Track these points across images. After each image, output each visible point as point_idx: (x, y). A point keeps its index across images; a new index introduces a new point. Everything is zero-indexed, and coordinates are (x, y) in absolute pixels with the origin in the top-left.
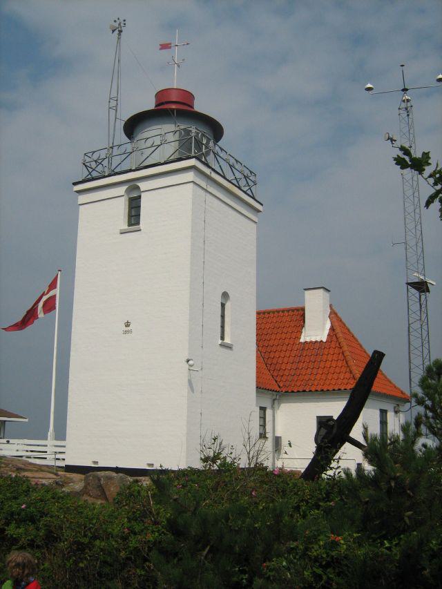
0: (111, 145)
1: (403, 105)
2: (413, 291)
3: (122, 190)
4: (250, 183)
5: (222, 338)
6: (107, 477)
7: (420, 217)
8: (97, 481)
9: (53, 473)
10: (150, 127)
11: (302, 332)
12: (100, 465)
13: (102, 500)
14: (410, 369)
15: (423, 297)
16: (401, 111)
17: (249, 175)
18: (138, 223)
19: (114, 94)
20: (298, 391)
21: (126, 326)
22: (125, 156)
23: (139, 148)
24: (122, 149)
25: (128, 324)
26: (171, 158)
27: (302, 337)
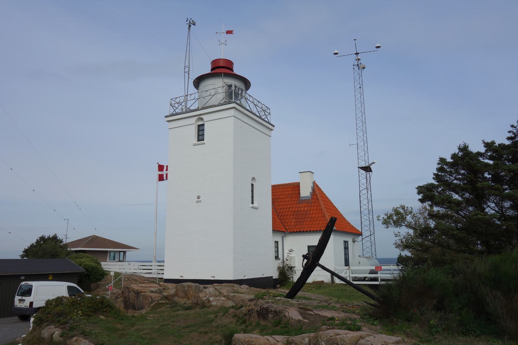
0: (186, 94)
1: (356, 63)
2: (363, 172)
4: (267, 114)
5: (252, 203)
6: (188, 286)
7: (362, 81)
12: (184, 278)
14: (360, 201)
15: (368, 175)
17: (266, 109)
18: (203, 140)
19: (187, 64)
20: (297, 232)
21: (198, 198)
22: (194, 101)
23: (219, 93)
24: (193, 97)
25: (199, 197)
26: (222, 102)
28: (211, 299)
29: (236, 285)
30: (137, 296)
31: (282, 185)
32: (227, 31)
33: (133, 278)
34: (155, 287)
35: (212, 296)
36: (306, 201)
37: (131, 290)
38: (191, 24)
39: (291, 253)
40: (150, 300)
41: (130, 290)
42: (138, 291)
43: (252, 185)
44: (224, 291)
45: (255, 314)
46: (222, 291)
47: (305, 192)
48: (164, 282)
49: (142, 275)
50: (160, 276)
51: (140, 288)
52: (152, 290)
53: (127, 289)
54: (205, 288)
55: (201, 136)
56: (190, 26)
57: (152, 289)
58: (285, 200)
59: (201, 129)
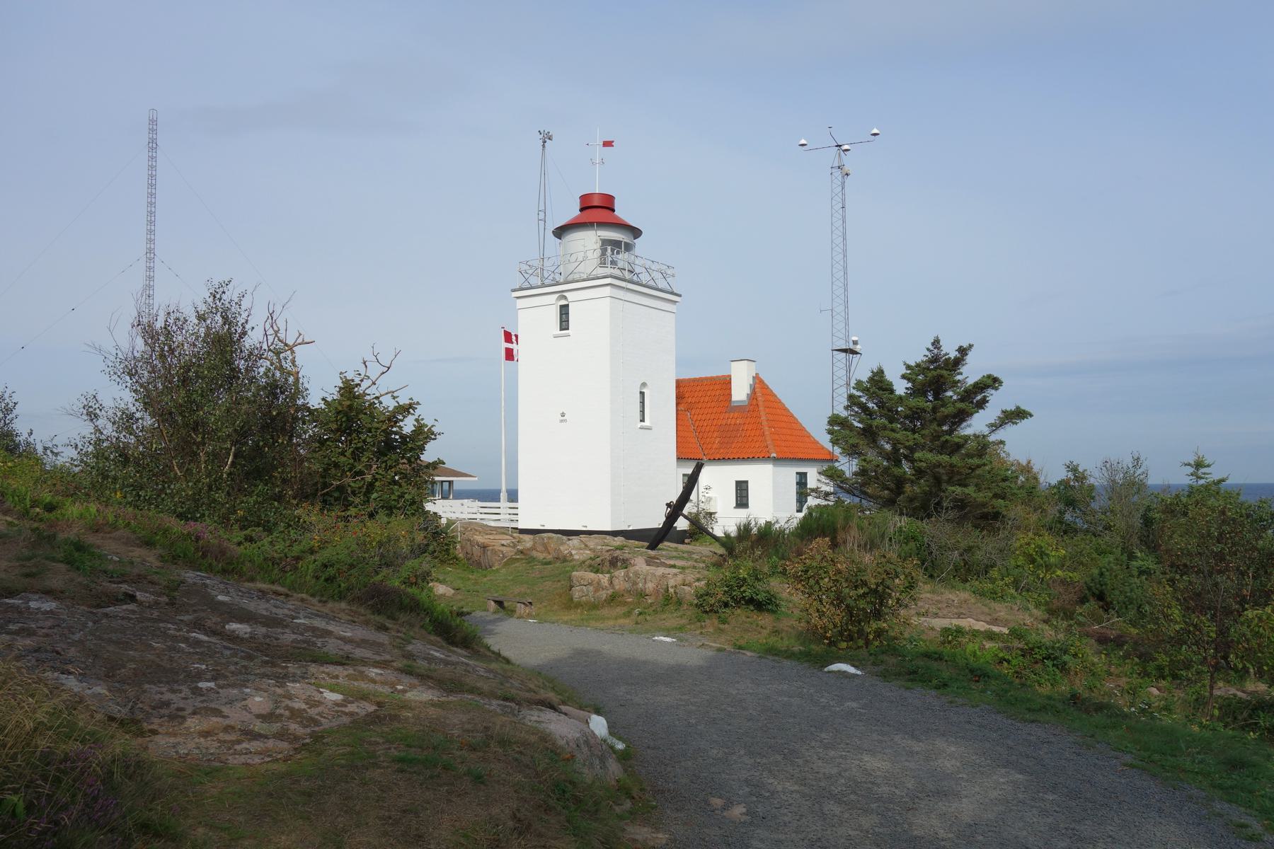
5: (643, 420)
8: (541, 540)
16: (834, 170)
18: (568, 329)
19: (542, 208)
25: (563, 415)
28: (573, 552)
29: (608, 537)
30: (484, 551)
31: (706, 378)
32: (604, 142)
34: (506, 540)
35: (576, 549)
36: (740, 408)
38: (547, 138)
39: (707, 491)
43: (642, 394)
44: (591, 545)
45: (607, 564)
46: (588, 543)
47: (740, 393)
49: (485, 523)
50: (514, 525)
51: (486, 541)
54: (569, 540)
55: (564, 324)
56: (545, 142)
57: (503, 542)
58: (709, 405)
59: (564, 310)
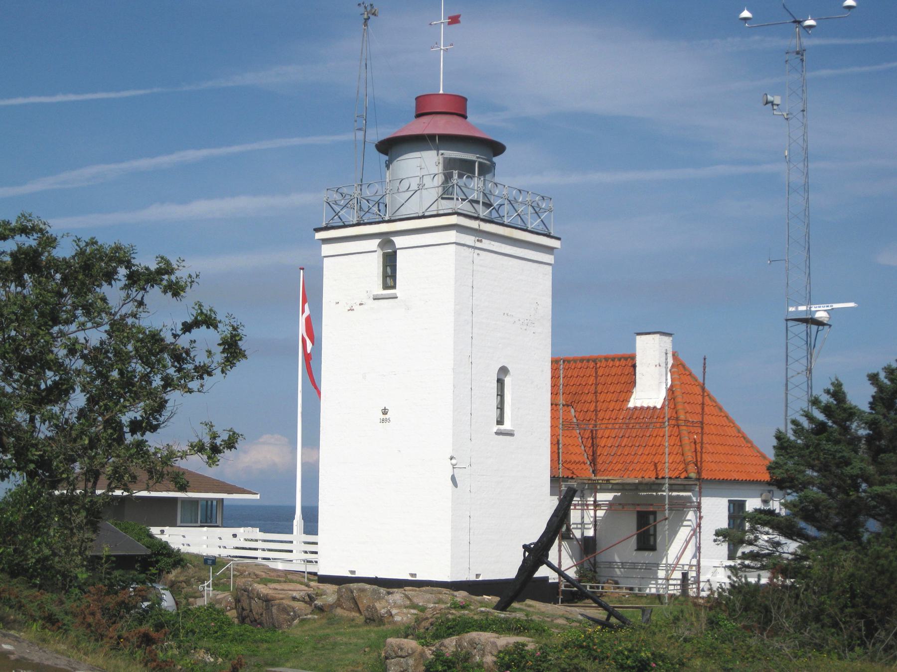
3: (374, 244)
5: (500, 422)
8: (349, 594)
9: (302, 583)
10: (406, 155)
11: (633, 392)
12: (358, 575)
13: (356, 612)
18: (394, 287)
21: (383, 414)
23: (426, 187)
25: (385, 412)
27: (632, 400)
28: (394, 611)
33: (251, 570)
34: (299, 591)
37: (253, 594)
40: (292, 613)
41: (251, 595)
42: (269, 597)
48: (319, 582)
50: (311, 568)
51: (271, 592)
52: (294, 595)
53: (246, 593)
54: (389, 593)
57: (295, 594)
59: (390, 261)
